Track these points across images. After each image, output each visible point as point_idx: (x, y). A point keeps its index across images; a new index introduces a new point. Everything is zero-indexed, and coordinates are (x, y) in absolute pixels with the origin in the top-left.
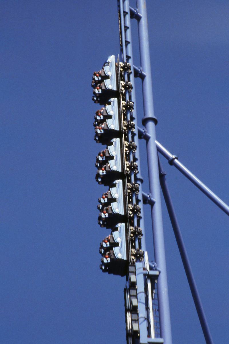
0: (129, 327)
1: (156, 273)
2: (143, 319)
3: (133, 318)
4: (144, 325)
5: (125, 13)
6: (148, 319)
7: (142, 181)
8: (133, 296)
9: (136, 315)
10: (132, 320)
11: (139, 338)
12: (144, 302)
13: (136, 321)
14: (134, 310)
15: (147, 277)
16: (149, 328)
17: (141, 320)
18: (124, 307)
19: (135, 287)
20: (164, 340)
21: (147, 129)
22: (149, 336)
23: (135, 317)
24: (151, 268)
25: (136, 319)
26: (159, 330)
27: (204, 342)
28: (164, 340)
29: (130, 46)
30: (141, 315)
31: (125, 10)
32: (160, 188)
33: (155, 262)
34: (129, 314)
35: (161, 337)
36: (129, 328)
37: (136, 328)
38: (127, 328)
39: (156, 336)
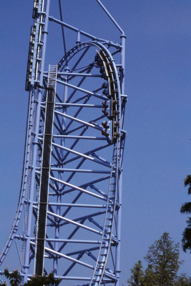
0: (35, 7)
1: (42, 44)
2: (40, 5)
3: (33, 39)
4: (40, 7)
5: (32, 102)
6: (42, 5)
7: (32, 126)
8: (34, 31)
9: (34, 38)
10: (36, 4)
11: (37, 11)
12: (38, 34)
13: (34, 40)
14: (34, 36)
15: (40, 24)
16: (41, 8)
17: (39, 5)
18: (26, 78)
19: (34, 45)
20: (45, 24)
21: (35, 132)
22: (41, 11)
23: (37, 3)
24: (41, 42)
25: (38, 4)
26: (45, 5)
27: (61, 1)
28: (45, 24)
29: (31, 117)
30: (39, 3)
31: (30, 121)
32: (35, 180)
33: (43, 39)
34: (35, 3)
35: (45, 12)
36: (34, 7)
37: (37, 7)
38: (34, 7)
39: (39, 58)
